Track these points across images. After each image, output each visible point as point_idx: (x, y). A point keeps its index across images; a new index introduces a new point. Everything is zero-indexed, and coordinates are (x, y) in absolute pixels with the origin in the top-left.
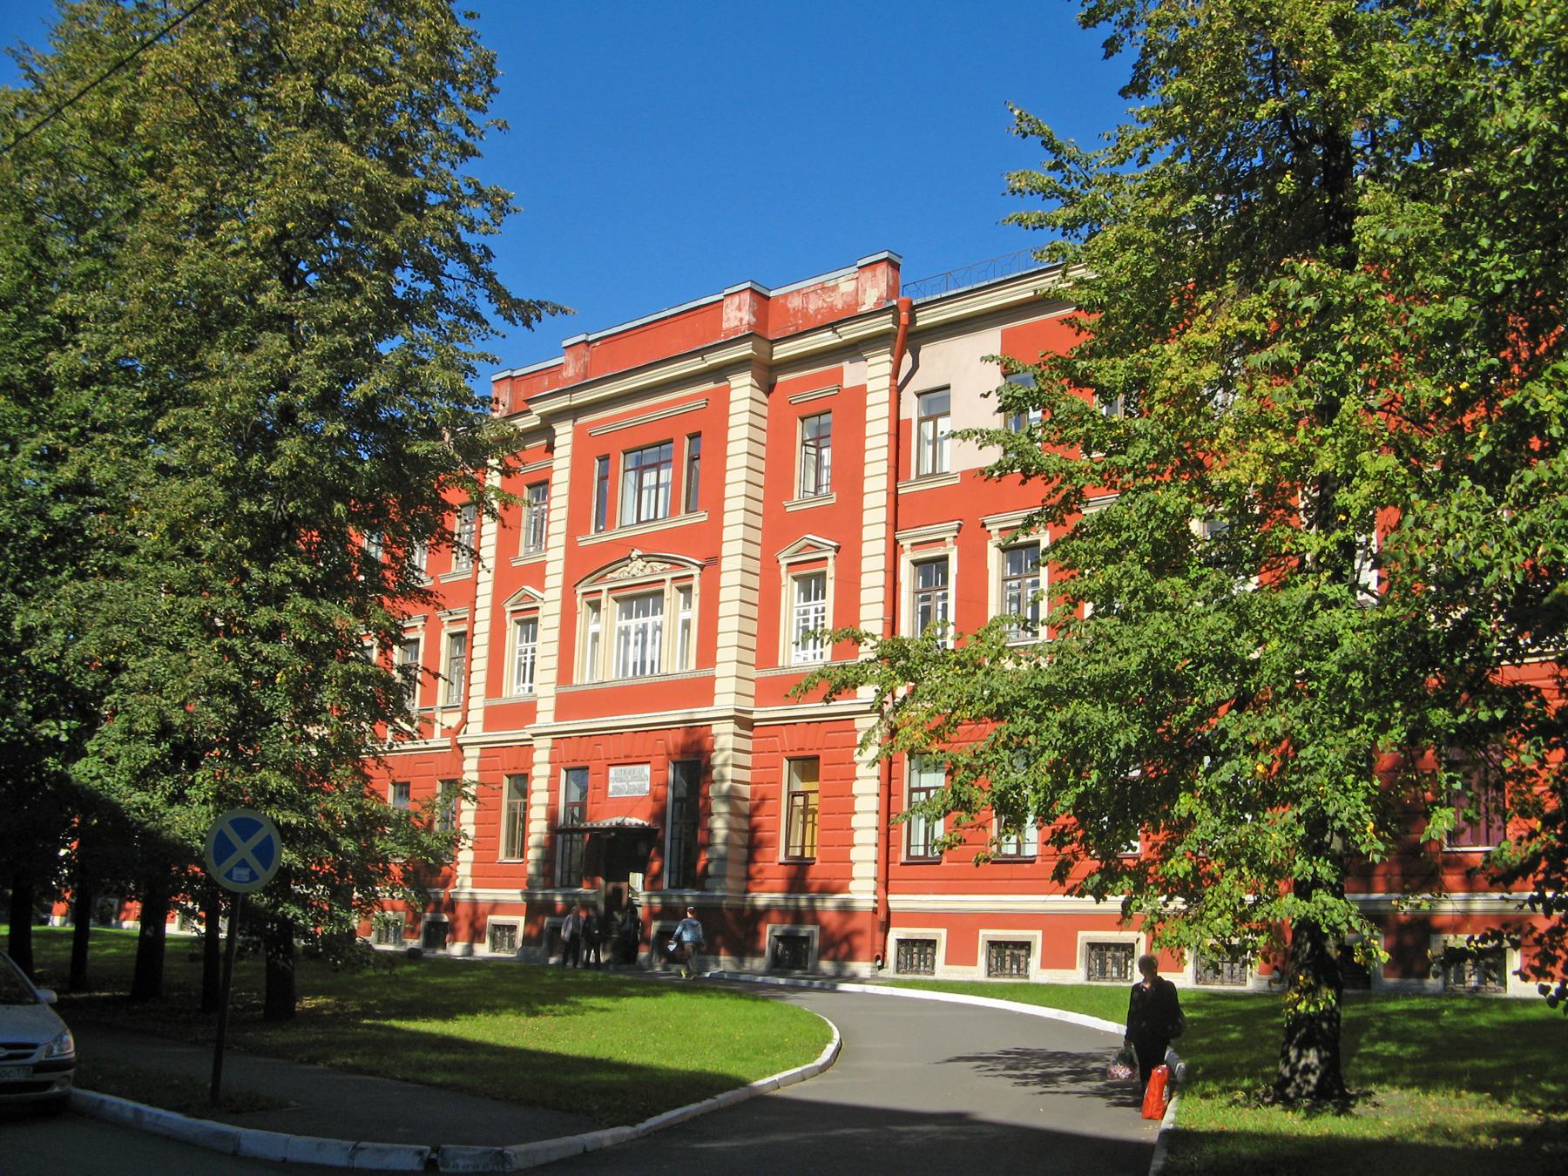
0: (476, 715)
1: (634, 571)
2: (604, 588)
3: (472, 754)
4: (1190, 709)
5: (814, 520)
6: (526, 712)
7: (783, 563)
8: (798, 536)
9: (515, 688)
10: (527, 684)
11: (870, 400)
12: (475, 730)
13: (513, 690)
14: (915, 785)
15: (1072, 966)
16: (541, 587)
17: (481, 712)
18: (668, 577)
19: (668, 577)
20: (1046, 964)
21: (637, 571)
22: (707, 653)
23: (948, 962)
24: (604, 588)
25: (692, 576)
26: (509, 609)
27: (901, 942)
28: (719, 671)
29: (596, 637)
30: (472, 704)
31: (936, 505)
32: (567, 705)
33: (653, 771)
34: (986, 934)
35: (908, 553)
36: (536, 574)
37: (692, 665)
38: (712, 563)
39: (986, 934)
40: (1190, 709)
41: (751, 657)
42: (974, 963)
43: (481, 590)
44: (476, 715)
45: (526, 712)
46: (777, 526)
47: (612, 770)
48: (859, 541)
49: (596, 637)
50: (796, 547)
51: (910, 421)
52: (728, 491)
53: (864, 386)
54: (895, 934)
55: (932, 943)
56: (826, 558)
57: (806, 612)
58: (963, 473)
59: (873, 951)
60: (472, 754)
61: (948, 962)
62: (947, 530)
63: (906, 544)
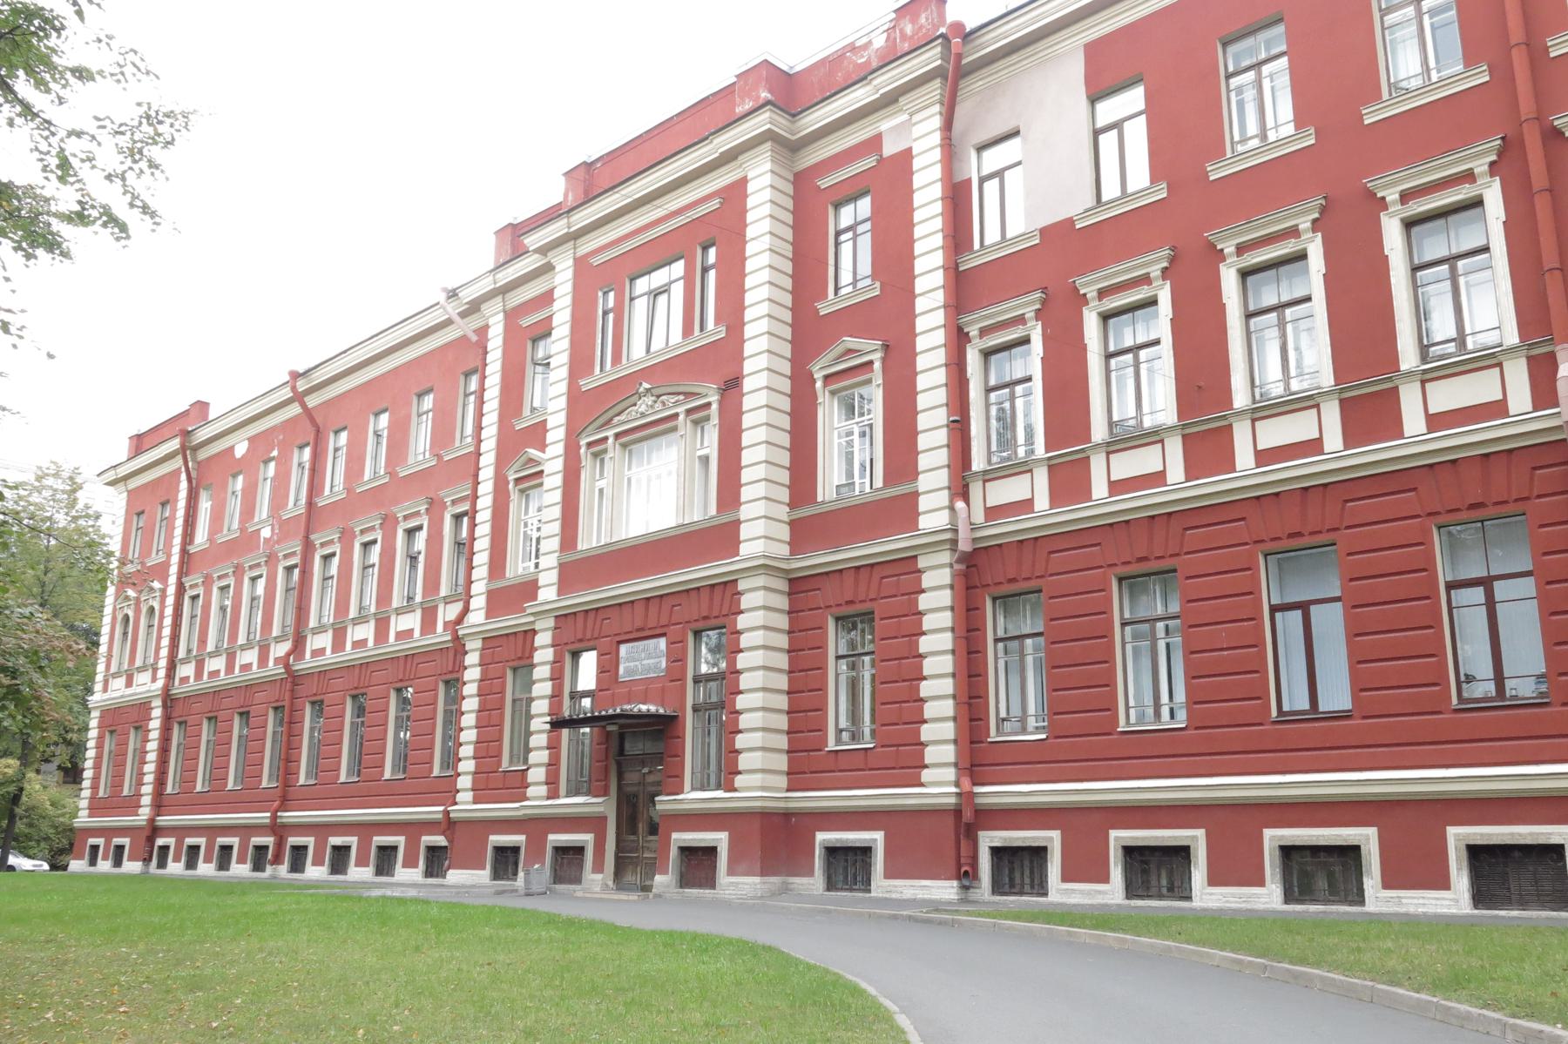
0: (479, 602)
1: (643, 409)
2: (610, 433)
3: (473, 645)
4: (94, 723)
5: (859, 317)
6: (529, 588)
7: (818, 376)
8: (835, 338)
9: (521, 566)
10: (534, 561)
11: (917, 164)
12: (477, 617)
13: (518, 568)
14: (1001, 633)
15: (1443, 883)
16: (542, 447)
17: (484, 597)
18: (681, 409)
19: (681, 409)
20: (1216, 878)
21: (645, 408)
22: (729, 492)
23: (1066, 878)
24: (610, 433)
25: (709, 405)
26: (512, 477)
27: (996, 852)
28: (745, 512)
29: (601, 491)
30: (475, 588)
31: (1012, 271)
32: (573, 573)
33: (670, 644)
34: (1120, 837)
35: (976, 341)
36: (537, 434)
37: (713, 511)
38: (732, 386)
39: (1120, 837)
40: (94, 723)
41: (784, 495)
42: (1443, 883)
43: (483, 461)
44: (479, 602)
45: (529, 588)
46: (808, 331)
47: (623, 649)
48: (912, 334)
49: (601, 491)
50: (832, 355)
51: (969, 181)
52: (749, 298)
53: (910, 150)
54: (988, 839)
55: (1040, 853)
56: (871, 363)
57: (850, 433)
58: (1043, 231)
59: (959, 866)
60: (473, 645)
61: (1066, 878)
62: (1027, 305)
63: (973, 332)
